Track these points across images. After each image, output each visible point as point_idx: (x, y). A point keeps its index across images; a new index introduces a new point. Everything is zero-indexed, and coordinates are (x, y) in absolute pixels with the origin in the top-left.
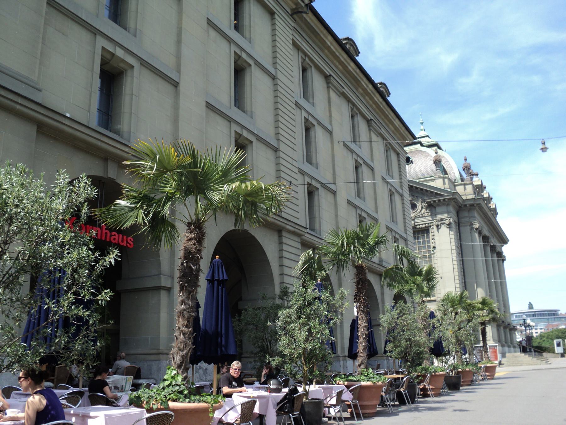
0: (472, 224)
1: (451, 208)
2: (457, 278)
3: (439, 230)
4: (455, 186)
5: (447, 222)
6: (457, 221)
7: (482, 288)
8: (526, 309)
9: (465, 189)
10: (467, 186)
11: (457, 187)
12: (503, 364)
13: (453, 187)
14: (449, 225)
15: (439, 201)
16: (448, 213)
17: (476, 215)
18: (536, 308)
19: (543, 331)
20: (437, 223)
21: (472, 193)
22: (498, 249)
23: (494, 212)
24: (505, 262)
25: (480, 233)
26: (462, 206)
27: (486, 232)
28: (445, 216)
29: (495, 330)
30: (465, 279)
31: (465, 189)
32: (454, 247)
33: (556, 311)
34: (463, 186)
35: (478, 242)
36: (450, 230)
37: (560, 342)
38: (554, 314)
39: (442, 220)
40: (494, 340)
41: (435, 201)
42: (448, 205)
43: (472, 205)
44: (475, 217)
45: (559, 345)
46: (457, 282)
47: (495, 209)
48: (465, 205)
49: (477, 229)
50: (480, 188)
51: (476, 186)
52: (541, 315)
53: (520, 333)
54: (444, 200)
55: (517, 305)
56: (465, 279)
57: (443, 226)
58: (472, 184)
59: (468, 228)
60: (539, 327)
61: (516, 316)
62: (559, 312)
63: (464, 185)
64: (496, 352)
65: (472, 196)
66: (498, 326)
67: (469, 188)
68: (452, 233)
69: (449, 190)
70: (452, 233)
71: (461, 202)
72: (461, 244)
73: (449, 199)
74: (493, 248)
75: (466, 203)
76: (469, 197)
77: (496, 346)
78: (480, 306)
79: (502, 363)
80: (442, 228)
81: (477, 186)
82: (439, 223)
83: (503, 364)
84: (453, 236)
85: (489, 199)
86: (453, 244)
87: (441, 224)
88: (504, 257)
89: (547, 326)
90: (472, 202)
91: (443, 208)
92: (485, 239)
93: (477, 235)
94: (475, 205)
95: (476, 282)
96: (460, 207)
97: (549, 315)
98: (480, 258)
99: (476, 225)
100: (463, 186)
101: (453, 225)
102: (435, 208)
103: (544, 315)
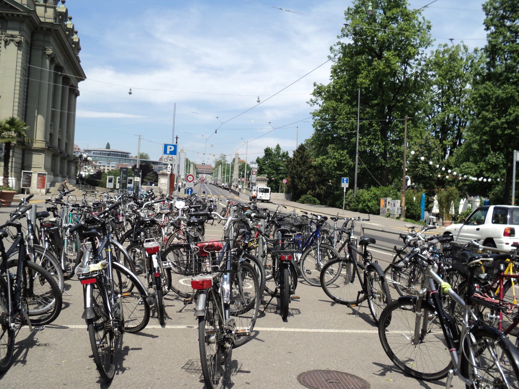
0: (45, 49)
1: (25, 27)
2: (17, 100)
3: (7, 47)
4: (35, 5)
5: (17, 39)
6: (29, 42)
7: (43, 116)
8: (103, 148)
9: (46, 11)
10: (48, 9)
11: (37, 7)
12: (50, 193)
13: (33, 6)
14: (19, 44)
15: (13, 15)
16: (20, 30)
17: (51, 40)
18: (113, 148)
19: (113, 168)
20: (6, 38)
21: (52, 17)
22: (73, 82)
23: (77, 47)
24: (78, 97)
25: (52, 60)
26: (39, 28)
27: (61, 60)
28: (16, 33)
29: (49, 159)
30: (26, 103)
31: (46, 11)
32: (19, 68)
33: (128, 153)
34: (44, 8)
35: (47, 68)
36: (19, 49)
37: (112, 179)
38: (126, 156)
39: (12, 36)
40: (45, 168)
41: (7, 14)
42: (22, 22)
43: (49, 30)
44: (50, 42)
45: (110, 181)
46: (16, 104)
47: (77, 44)
48: (42, 28)
49: (49, 55)
50: (64, 16)
51: (59, 12)
52: (115, 155)
53: (94, 168)
54: (18, 15)
55: (84, 141)
56: (26, 103)
57: (12, 43)
58: (55, 8)
59: (41, 52)
60: (111, 165)
61: (94, 153)
62: (130, 155)
63: (46, 7)
64: (44, 180)
65: (52, 21)
66: (54, 157)
67: (50, 12)
68: (20, 52)
69: (26, 6)
70: (20, 52)
71: (37, 23)
72: (29, 67)
73: (23, 16)
74: (66, 80)
75: (43, 26)
76: (48, 21)
77: (45, 174)
78: (8, 126)
79: (50, 191)
80: (10, 45)
81: (61, 13)
82: (9, 39)
83: (50, 193)
84: (20, 56)
85: (72, 31)
86: (20, 64)
87: (10, 40)
88: (78, 92)
89: (118, 165)
90: (49, 27)
91: (16, 25)
92: (58, 68)
93: (48, 62)
94: (52, 30)
95: (38, 109)
96: (36, 28)
97: (122, 156)
98: (47, 83)
99: (50, 52)
100: (44, 8)
101: (24, 45)
102: (7, 21)
103: (117, 155)
